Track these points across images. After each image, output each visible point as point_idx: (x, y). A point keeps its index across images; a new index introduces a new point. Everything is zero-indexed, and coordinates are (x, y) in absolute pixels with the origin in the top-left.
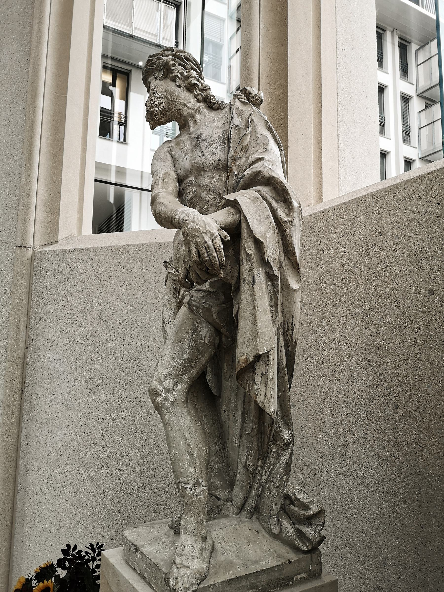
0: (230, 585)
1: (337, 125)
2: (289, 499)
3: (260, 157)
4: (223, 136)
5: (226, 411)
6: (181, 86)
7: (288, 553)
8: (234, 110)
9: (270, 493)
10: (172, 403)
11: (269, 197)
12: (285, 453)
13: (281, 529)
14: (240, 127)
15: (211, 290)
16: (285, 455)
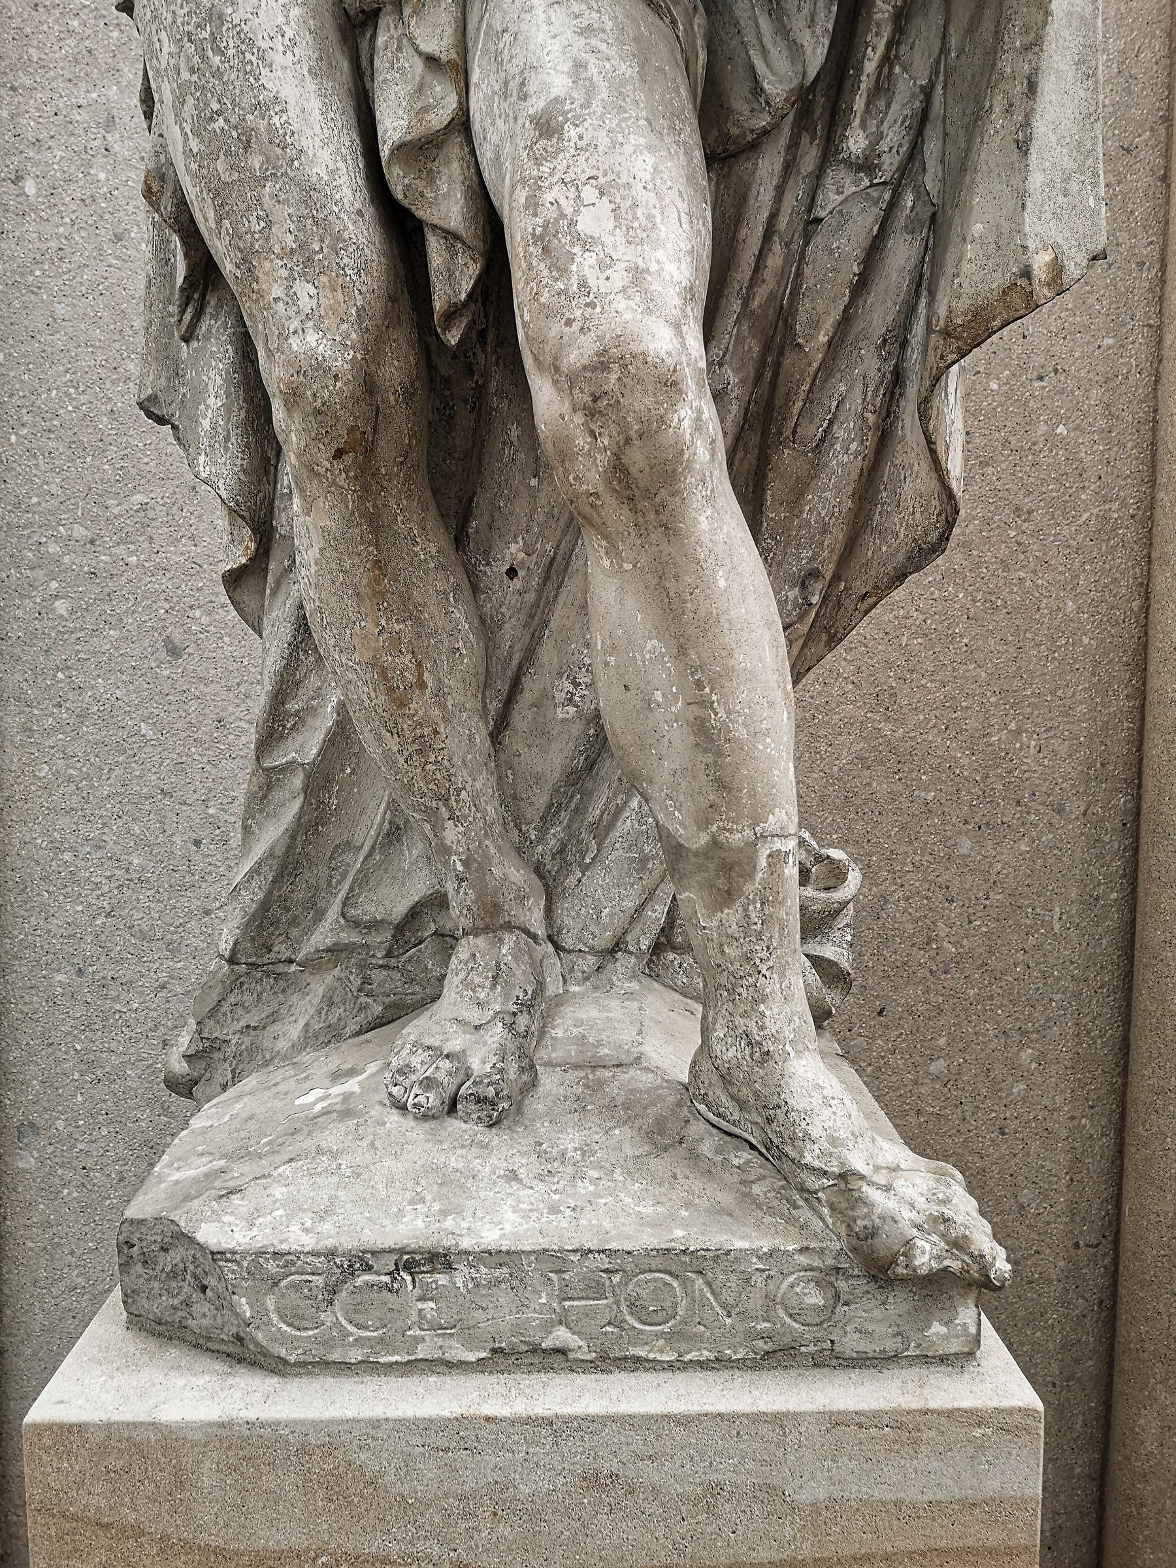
5: (521, 573)
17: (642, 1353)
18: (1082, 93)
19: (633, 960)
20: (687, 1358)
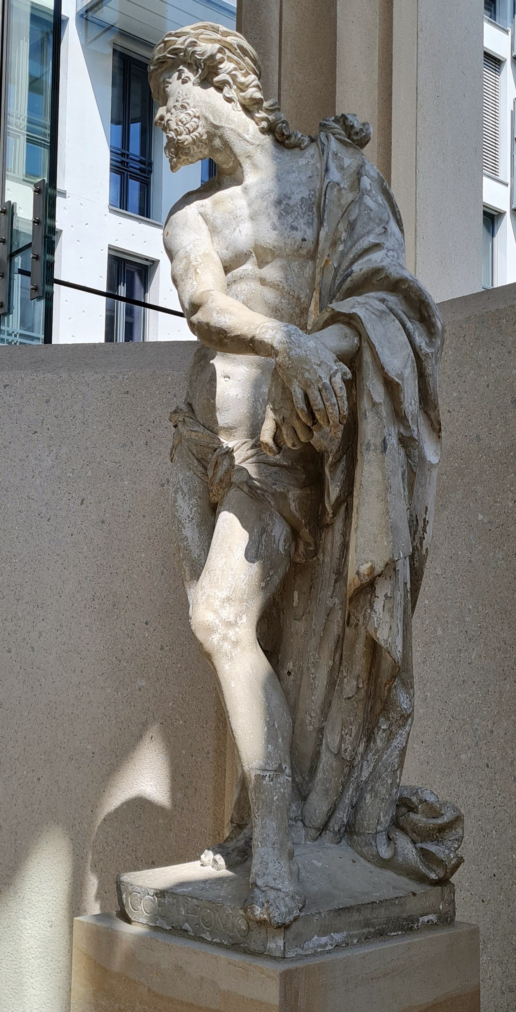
0: (339, 917)
1: (414, 156)
2: (405, 805)
3: (377, 241)
4: (309, 198)
5: (293, 674)
6: (233, 101)
7: (408, 885)
8: (330, 156)
9: (376, 796)
10: (235, 644)
11: (400, 312)
12: (400, 732)
13: (395, 849)
14: (342, 186)
15: (285, 463)
16: (401, 734)
17: (204, 936)
18: (380, 506)
19: (332, 834)
20: (214, 941)
